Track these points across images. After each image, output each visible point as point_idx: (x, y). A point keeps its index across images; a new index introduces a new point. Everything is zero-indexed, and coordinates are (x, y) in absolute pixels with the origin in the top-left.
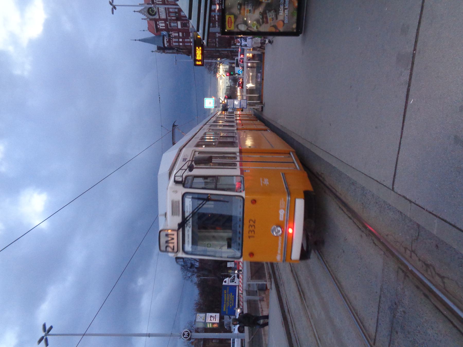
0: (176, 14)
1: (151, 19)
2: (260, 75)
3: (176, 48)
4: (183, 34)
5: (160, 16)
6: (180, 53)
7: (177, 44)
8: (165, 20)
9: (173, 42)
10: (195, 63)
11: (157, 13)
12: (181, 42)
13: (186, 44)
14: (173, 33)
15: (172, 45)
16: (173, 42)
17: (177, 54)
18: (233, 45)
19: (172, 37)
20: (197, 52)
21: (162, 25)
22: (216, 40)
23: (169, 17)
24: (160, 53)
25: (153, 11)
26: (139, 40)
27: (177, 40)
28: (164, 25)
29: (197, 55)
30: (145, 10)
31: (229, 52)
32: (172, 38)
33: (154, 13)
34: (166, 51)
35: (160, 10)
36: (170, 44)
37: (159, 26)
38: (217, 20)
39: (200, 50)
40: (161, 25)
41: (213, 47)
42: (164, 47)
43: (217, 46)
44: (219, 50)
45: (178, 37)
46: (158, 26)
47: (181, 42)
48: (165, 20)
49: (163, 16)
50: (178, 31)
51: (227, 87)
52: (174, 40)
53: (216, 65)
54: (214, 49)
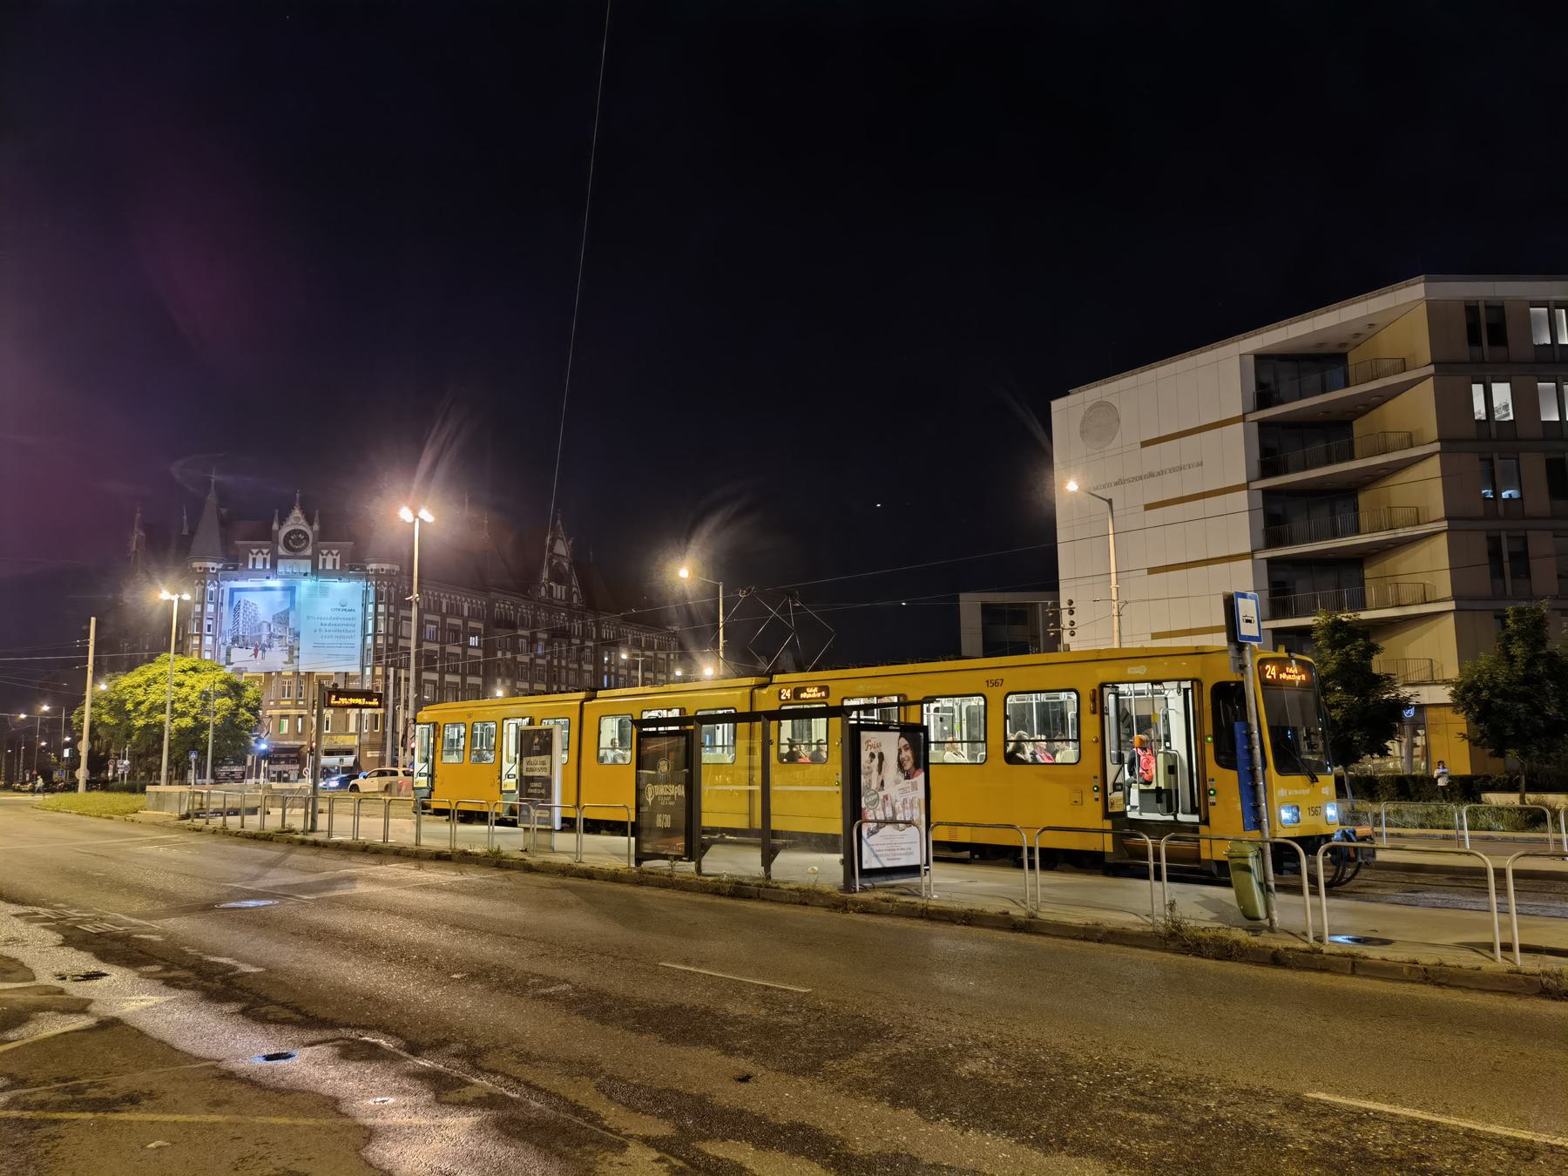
13: (605, 677)
33: (291, 544)
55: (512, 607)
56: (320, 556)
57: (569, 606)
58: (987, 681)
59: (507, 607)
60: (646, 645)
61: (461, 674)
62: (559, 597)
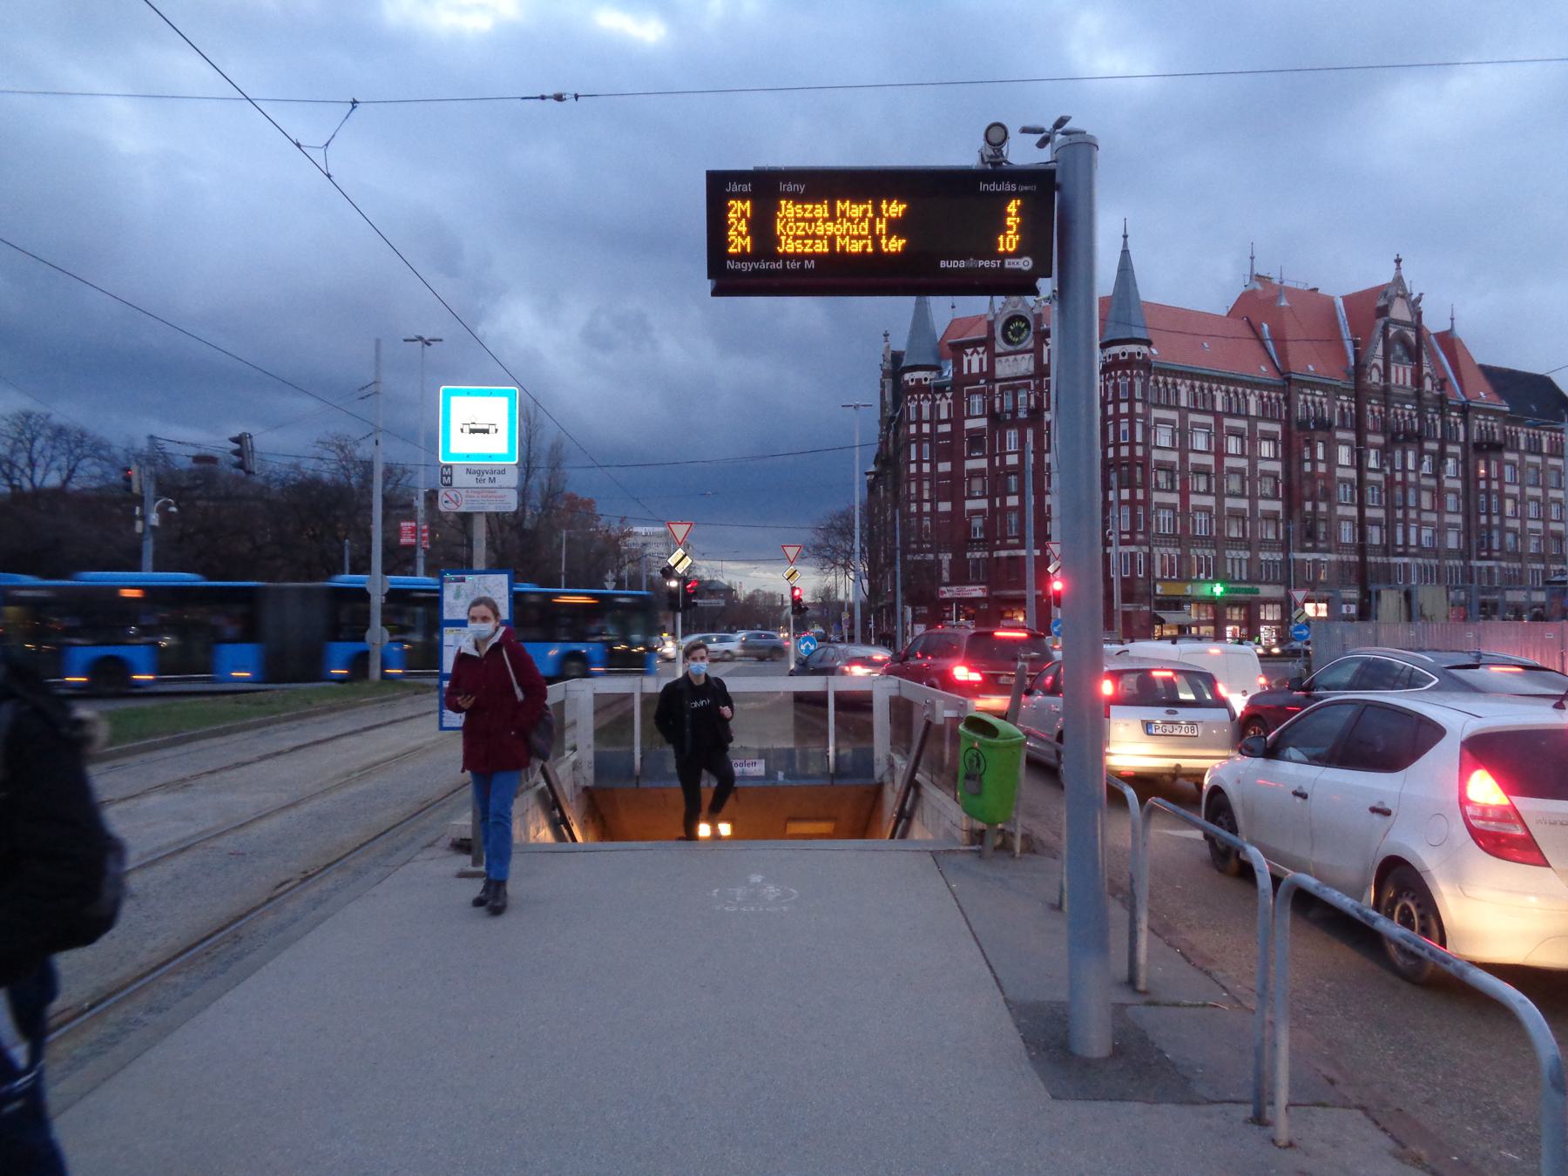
0: (1010, 412)
1: (991, 325)
2: (756, 774)
3: (897, 414)
4: (944, 435)
5: (1003, 359)
6: (882, 430)
7: (913, 417)
9: (1132, 379)
10: (735, 187)
11: (1010, 348)
12: (919, 428)
13: (913, 447)
14: (950, 401)
15: (909, 397)
16: (1132, 379)
17: (881, 422)
18: (913, 611)
19: (934, 400)
20: (856, 211)
21: (974, 362)
22: (929, 551)
23: (1000, 387)
24: (882, 362)
25: (1018, 332)
27: (926, 414)
28: (975, 369)
29: (821, 210)
30: (1020, 305)
31: (890, 601)
32: (933, 396)
33: (1011, 337)
34: (889, 382)
35: (1023, 358)
36: (912, 390)
37: (972, 354)
38: (995, 554)
39: (876, 240)
40: (975, 359)
41: (906, 543)
42: (905, 368)
43: (909, 557)
44: (895, 564)
45: (936, 418)
46: (969, 351)
47: (919, 428)
48: (989, 375)
49: (1004, 368)
50: (957, 419)
51: (782, 595)
52: (926, 405)
53: (846, 551)
54: (898, 545)
55: (1324, 400)
56: (1044, 345)
57: (1419, 396)
58: (1244, 275)
59: (1489, 423)
60: (1550, 447)
61: (1215, 495)
62: (1401, 383)
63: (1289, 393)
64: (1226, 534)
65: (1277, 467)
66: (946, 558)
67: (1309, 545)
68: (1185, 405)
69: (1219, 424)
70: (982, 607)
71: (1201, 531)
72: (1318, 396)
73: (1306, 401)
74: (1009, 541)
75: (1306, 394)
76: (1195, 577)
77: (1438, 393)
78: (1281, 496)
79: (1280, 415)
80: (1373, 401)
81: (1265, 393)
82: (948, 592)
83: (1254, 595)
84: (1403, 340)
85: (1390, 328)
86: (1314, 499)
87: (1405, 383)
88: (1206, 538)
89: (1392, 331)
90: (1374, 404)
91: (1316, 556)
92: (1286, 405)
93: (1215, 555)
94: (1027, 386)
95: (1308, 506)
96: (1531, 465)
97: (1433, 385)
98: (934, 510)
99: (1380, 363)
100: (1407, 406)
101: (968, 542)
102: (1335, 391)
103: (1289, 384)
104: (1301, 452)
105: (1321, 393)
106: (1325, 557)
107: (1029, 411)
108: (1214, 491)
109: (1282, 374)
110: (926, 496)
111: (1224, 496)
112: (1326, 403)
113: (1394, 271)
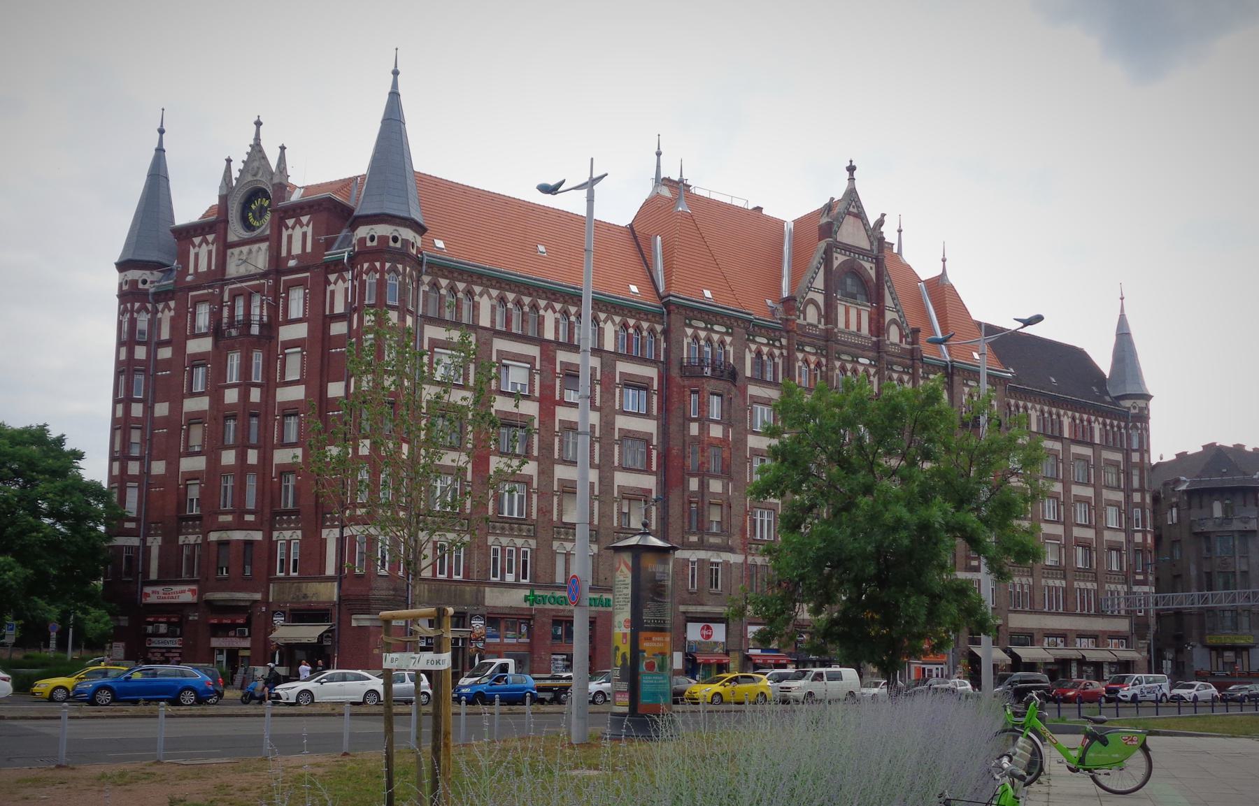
4: (167, 363)
8: (217, 276)
9: (382, 276)
15: (366, 265)
16: (382, 276)
19: (156, 311)
23: (231, 290)
26: (160, 150)
46: (197, 240)
48: (217, 276)
55: (728, 339)
56: (284, 229)
57: (878, 347)
62: (853, 328)
63: (669, 325)
64: (555, 518)
65: (649, 427)
66: (155, 543)
67: (694, 539)
68: (488, 325)
69: (548, 358)
70: (191, 618)
71: (512, 508)
72: (717, 332)
73: (696, 338)
74: (222, 518)
75: (697, 328)
76: (1078, 611)
77: (908, 347)
78: (654, 468)
79: (657, 355)
80: (807, 349)
81: (632, 322)
82: (155, 595)
83: (601, 609)
84: (854, 271)
85: (835, 255)
86: (704, 476)
87: (859, 329)
88: (519, 522)
89: (839, 259)
90: (809, 353)
91: (702, 554)
92: (666, 341)
93: (534, 547)
94: (259, 289)
95: (694, 484)
96: (1078, 457)
97: (901, 336)
98: (146, 471)
99: (820, 299)
100: (861, 360)
101: (182, 521)
102: (747, 329)
103: (669, 313)
104: (684, 404)
105: (723, 330)
106: (719, 556)
107: (262, 325)
108: (535, 453)
109: (661, 298)
110: (135, 452)
111: (554, 462)
112: (731, 344)
113: (847, 182)
